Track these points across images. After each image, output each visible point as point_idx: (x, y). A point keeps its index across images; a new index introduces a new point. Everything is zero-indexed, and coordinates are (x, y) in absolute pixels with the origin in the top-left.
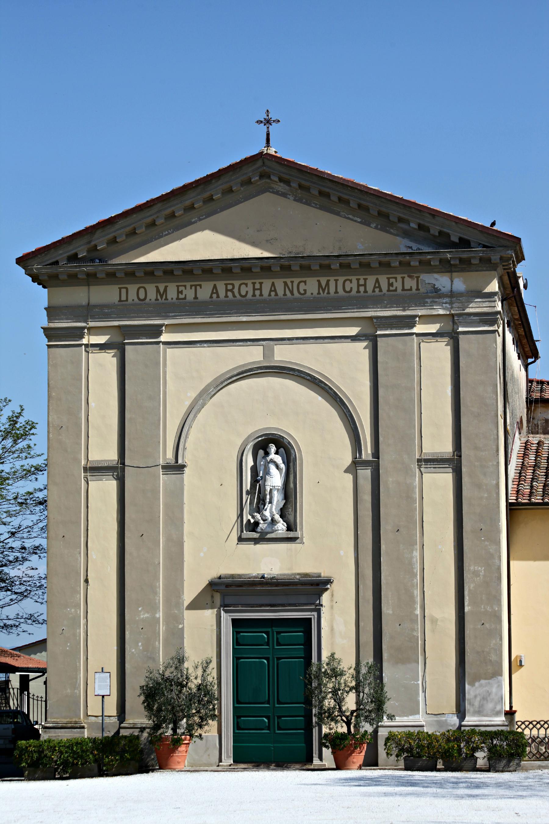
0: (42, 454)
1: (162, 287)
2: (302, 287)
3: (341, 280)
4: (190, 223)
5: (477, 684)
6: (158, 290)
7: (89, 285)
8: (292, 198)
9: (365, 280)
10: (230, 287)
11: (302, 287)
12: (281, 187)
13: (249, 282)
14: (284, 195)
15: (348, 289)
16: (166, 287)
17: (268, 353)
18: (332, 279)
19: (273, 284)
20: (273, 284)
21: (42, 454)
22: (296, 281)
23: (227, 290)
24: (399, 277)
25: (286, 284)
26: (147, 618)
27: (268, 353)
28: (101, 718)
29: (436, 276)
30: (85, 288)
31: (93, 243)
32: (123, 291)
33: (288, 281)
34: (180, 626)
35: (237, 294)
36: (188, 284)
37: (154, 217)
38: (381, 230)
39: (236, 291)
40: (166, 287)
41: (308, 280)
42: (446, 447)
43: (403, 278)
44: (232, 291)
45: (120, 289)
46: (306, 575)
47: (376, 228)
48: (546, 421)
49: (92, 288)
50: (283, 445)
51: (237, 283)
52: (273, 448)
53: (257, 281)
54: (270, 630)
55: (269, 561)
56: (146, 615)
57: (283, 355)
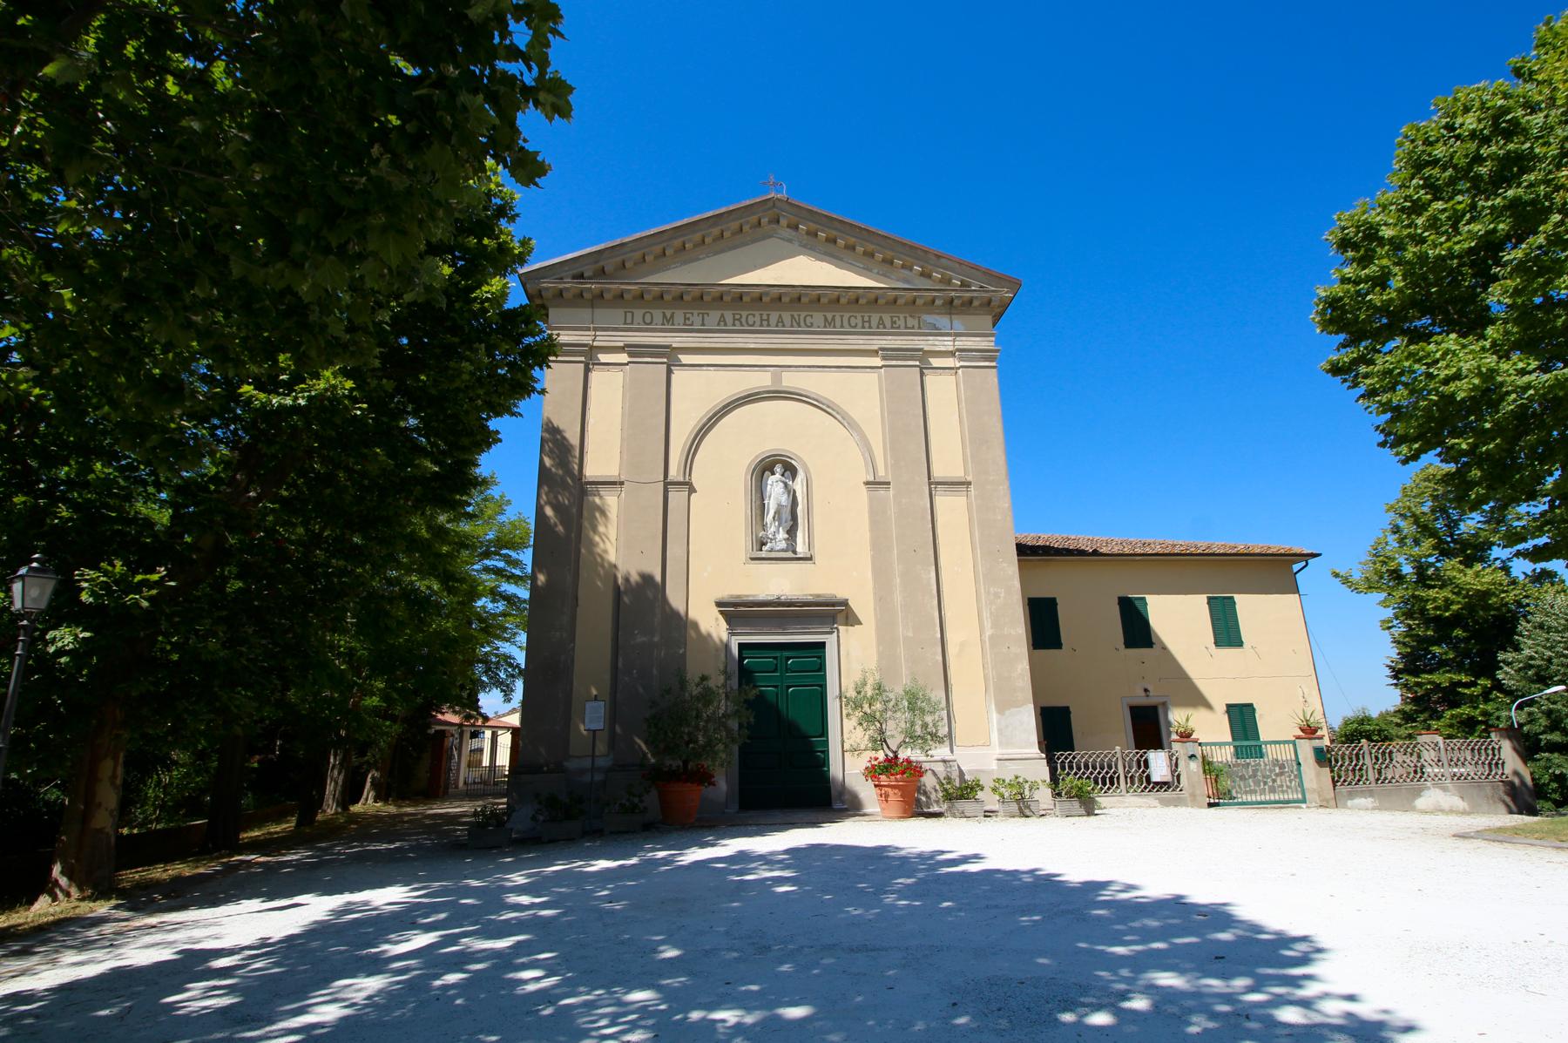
0: (1336, 575)
1: (829, 316)
2: (809, 320)
3: (846, 315)
4: (841, 259)
11: (809, 320)
12: (789, 233)
14: (790, 241)
17: (777, 379)
18: (838, 315)
21: (1336, 575)
22: (803, 314)
27: (777, 379)
30: (589, 310)
33: (829, 316)
41: (815, 314)
48: (1560, 778)
50: (790, 470)
52: (778, 469)
55: (776, 583)
57: (790, 381)
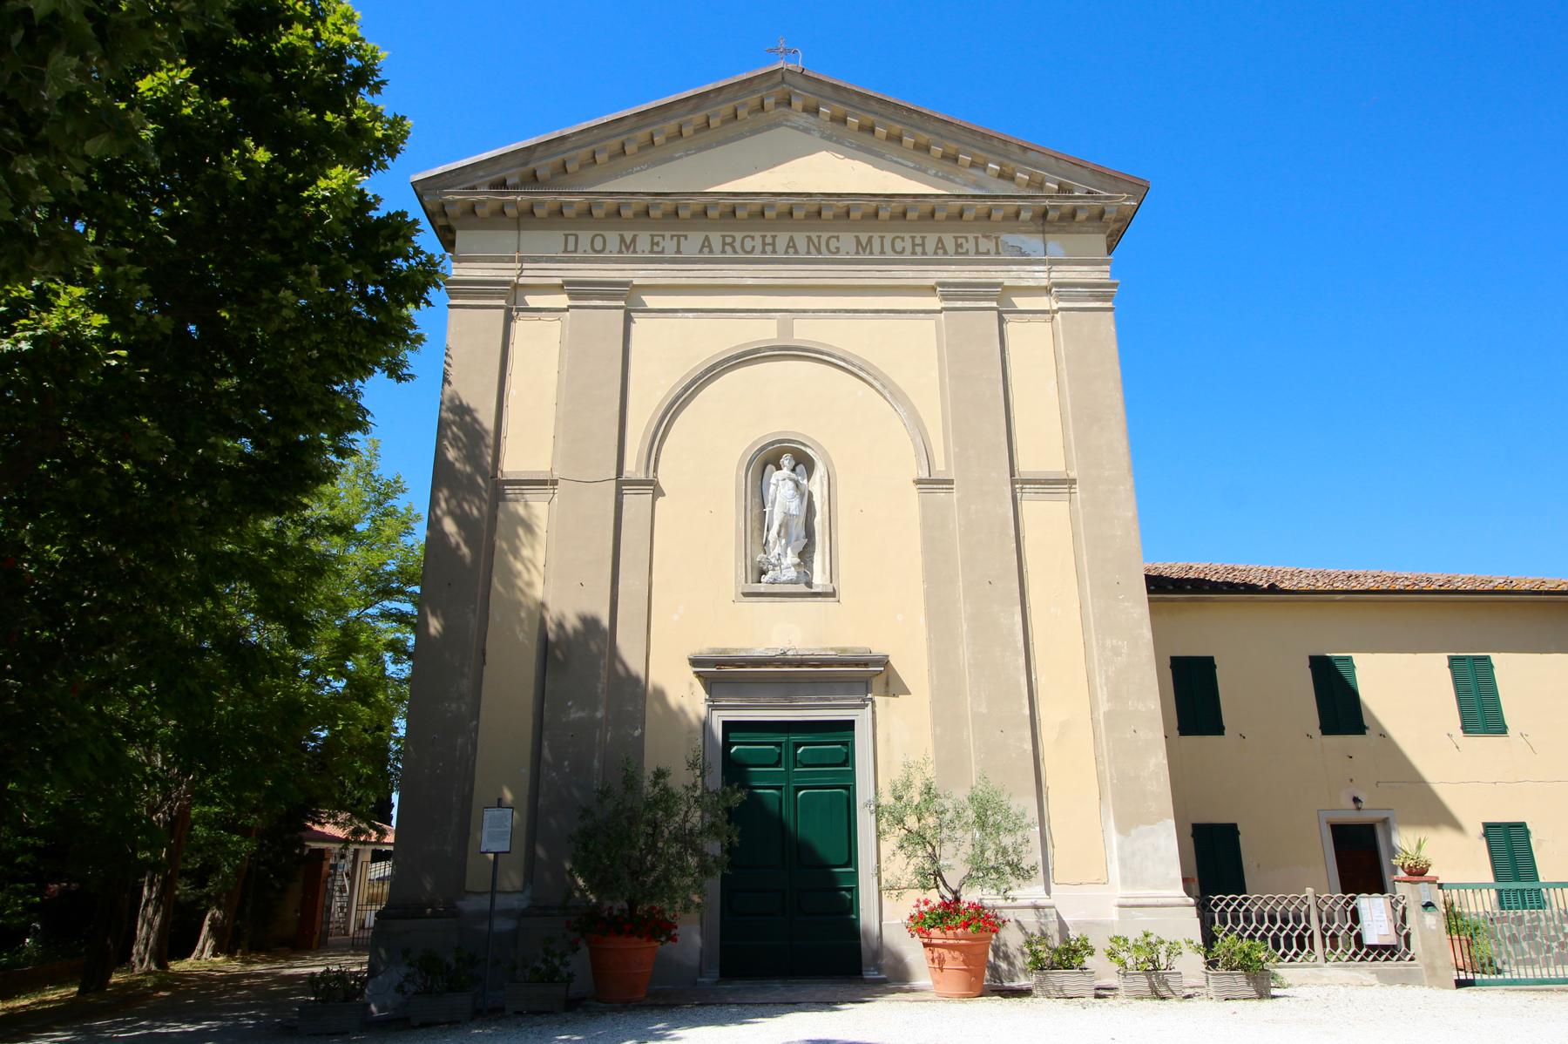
1: (628, 236)
3: (889, 237)
5: (1133, 832)
6: (623, 240)
7: (519, 229)
8: (817, 134)
9: (923, 238)
10: (728, 240)
13: (757, 235)
14: (807, 131)
15: (899, 249)
16: (635, 237)
18: (876, 236)
19: (791, 238)
20: (791, 238)
23: (724, 244)
24: (971, 236)
25: (809, 238)
26: (233, 552)
28: (488, 897)
29: (1023, 237)
31: (532, 166)
32: (571, 240)
33: (814, 235)
34: (637, 733)
35: (738, 248)
36: (668, 234)
37: (624, 137)
38: (943, 177)
39: (737, 245)
40: (635, 237)
42: (1034, 509)
43: (976, 239)
44: (731, 244)
45: (566, 236)
46: (844, 650)
47: (936, 175)
49: (525, 234)
50: (804, 462)
51: (739, 236)
52: (786, 461)
53: (769, 234)
54: (783, 739)
56: (581, 714)
57: (806, 332)
